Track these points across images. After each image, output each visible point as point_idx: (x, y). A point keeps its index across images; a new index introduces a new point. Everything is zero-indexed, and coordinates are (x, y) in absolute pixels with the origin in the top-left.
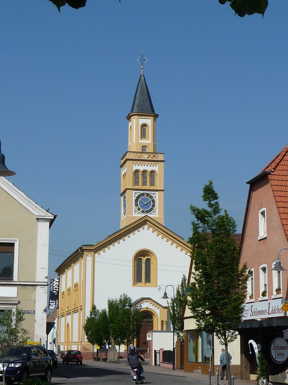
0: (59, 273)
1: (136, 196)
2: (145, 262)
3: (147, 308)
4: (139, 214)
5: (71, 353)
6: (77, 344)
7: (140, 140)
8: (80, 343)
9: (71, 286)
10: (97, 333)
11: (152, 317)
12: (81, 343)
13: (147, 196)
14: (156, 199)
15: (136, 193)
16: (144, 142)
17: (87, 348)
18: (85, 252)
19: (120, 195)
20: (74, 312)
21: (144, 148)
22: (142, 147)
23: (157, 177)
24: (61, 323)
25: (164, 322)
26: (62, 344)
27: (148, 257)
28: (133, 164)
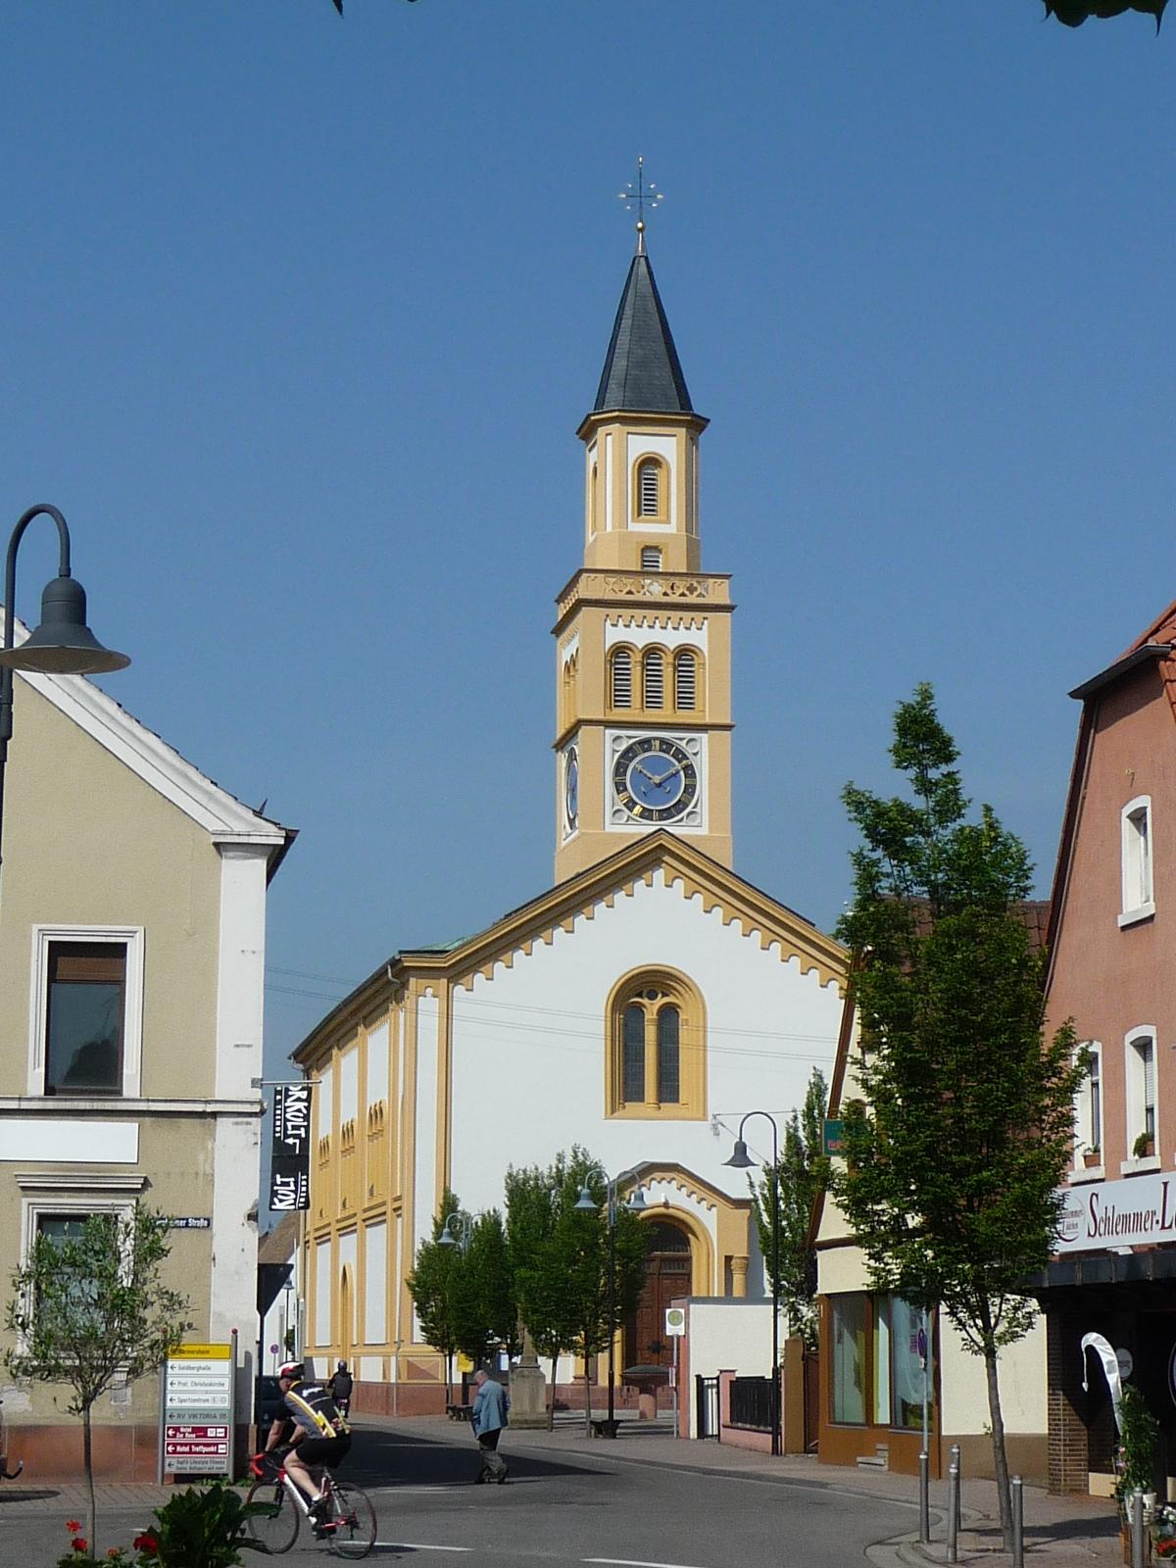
3: (666, 1205)
7: (633, 521)
15: (617, 738)
16: (648, 529)
18: (412, 981)
23: (704, 673)
25: (733, 1262)
27: (666, 1000)
28: (606, 620)
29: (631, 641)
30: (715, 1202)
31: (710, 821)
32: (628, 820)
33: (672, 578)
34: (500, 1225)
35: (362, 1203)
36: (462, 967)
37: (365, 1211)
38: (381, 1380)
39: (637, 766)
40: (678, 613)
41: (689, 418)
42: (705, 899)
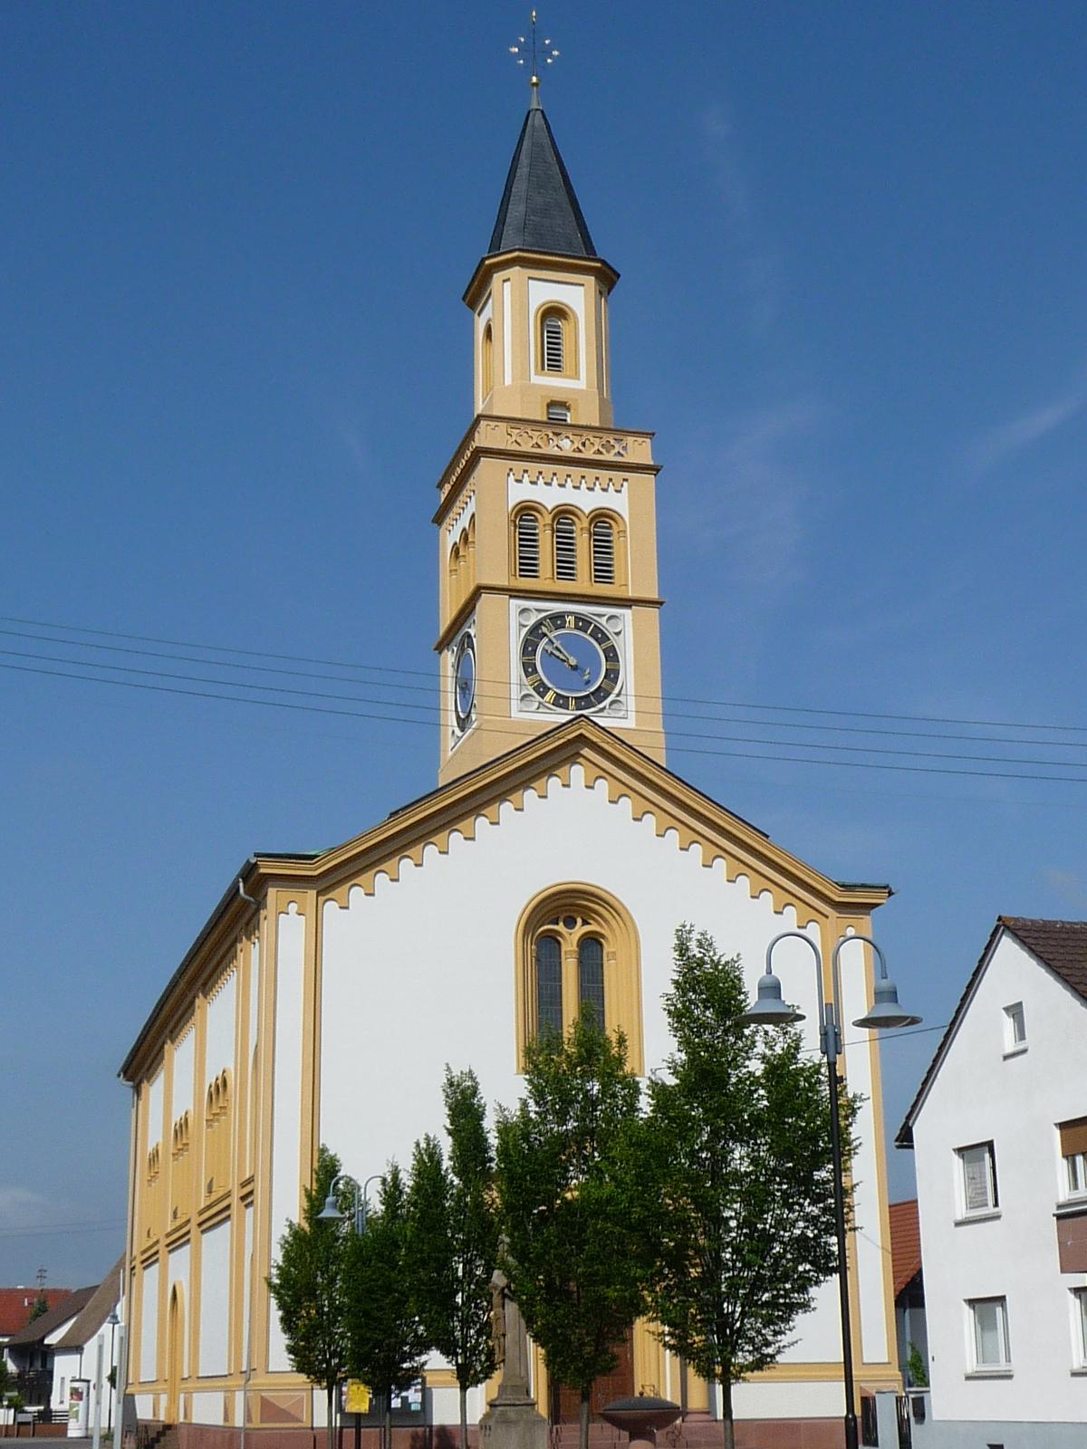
0: (137, 1081)
1: (525, 623)
2: (576, 949)
4: (540, 710)
6: (220, 1384)
8: (243, 1382)
9: (192, 1108)
10: (366, 1314)
12: (249, 1380)
13: (577, 627)
14: (622, 644)
15: (524, 611)
16: (555, 383)
18: (272, 892)
19: (435, 649)
20: (204, 1226)
21: (557, 414)
22: (545, 407)
23: (626, 542)
24: (141, 1310)
26: (148, 1387)
27: (587, 928)
28: (509, 475)
32: (538, 708)
33: (585, 433)
34: (439, 1163)
35: (198, 1203)
36: (335, 878)
37: (201, 1213)
38: (220, 1422)
39: (547, 647)
41: (599, 265)
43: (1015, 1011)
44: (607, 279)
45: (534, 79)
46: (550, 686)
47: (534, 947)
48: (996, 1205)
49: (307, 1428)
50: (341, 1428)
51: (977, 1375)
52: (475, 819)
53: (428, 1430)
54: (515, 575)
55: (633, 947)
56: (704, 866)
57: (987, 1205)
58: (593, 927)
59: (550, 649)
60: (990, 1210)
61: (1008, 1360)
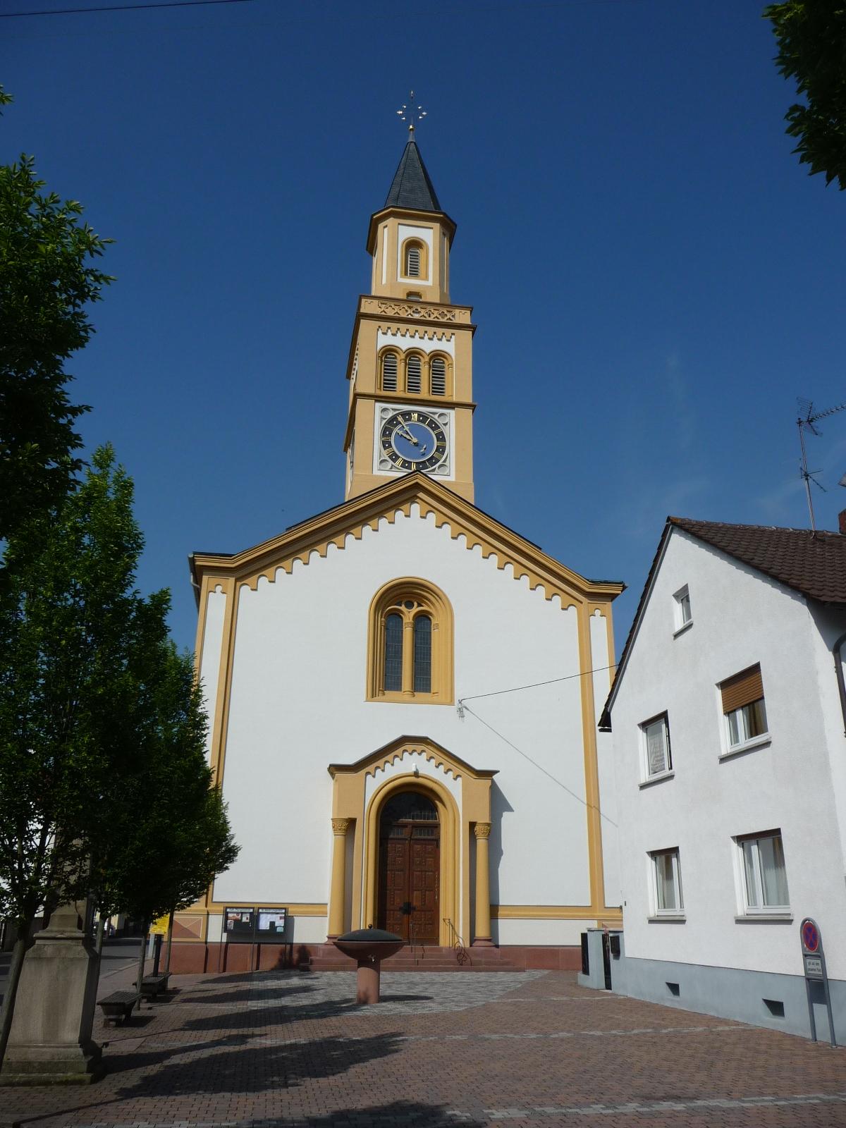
3: (416, 774)
4: (393, 470)
5: (281, 933)
7: (401, 277)
11: (434, 809)
15: (384, 410)
17: (186, 927)
23: (452, 370)
25: (477, 828)
28: (378, 330)
29: (397, 345)
30: (460, 772)
31: (457, 471)
36: (249, 569)
40: (433, 328)
41: (442, 216)
42: (515, 568)
43: (683, 596)
44: (449, 229)
45: (411, 127)
46: (399, 455)
47: (383, 619)
48: (671, 768)
49: (201, 942)
50: (227, 943)
51: (657, 918)
52: (345, 536)
53: (288, 946)
54: (380, 389)
55: (449, 619)
56: (499, 568)
57: (664, 769)
58: (425, 608)
59: (400, 433)
60: (667, 772)
61: (682, 906)
